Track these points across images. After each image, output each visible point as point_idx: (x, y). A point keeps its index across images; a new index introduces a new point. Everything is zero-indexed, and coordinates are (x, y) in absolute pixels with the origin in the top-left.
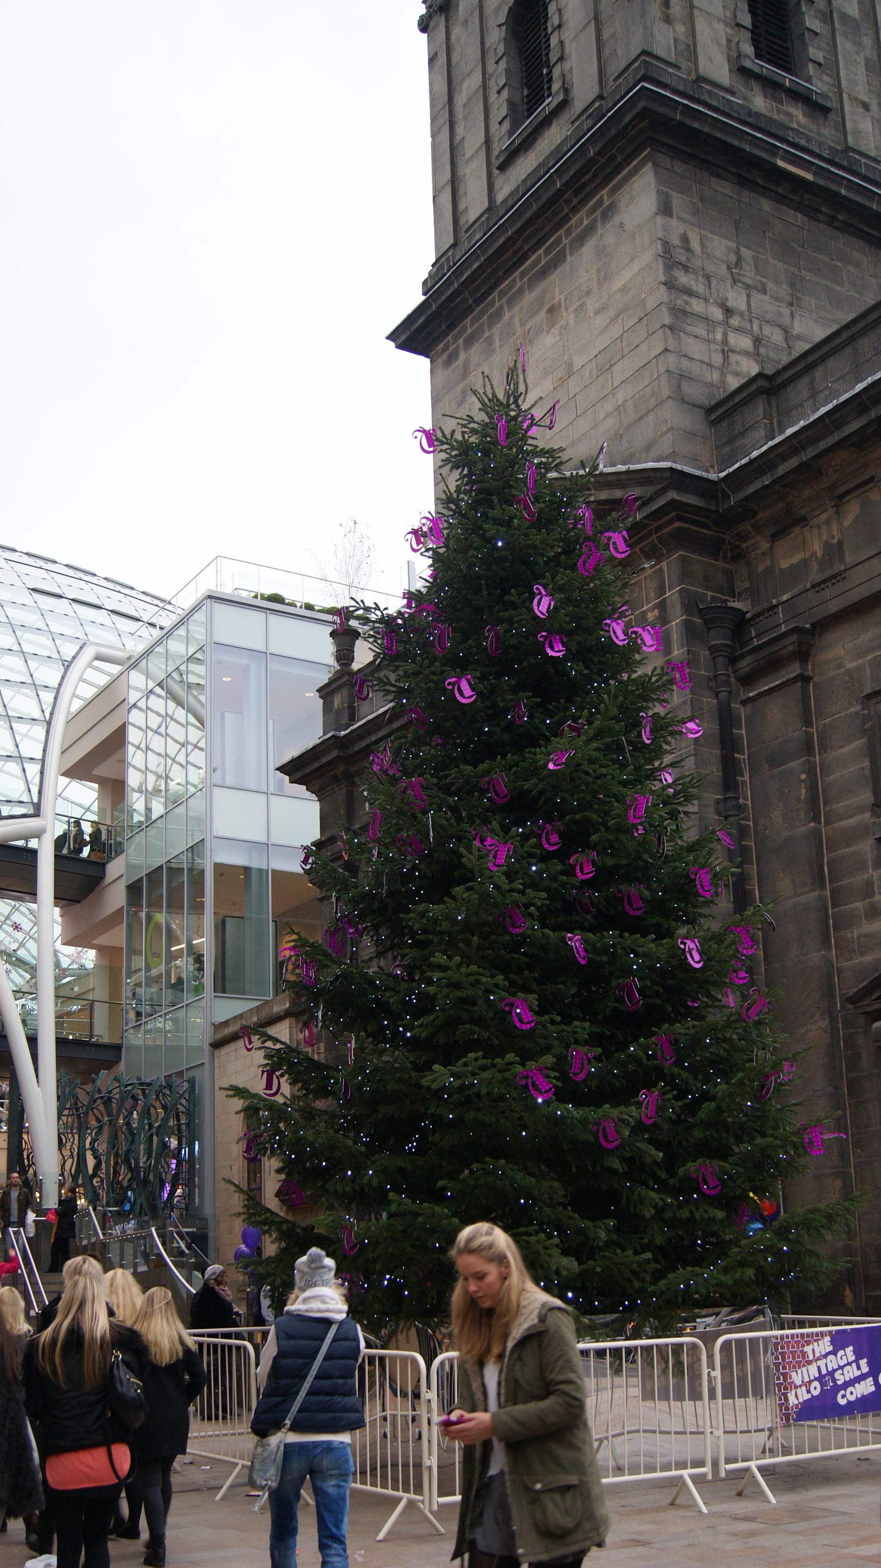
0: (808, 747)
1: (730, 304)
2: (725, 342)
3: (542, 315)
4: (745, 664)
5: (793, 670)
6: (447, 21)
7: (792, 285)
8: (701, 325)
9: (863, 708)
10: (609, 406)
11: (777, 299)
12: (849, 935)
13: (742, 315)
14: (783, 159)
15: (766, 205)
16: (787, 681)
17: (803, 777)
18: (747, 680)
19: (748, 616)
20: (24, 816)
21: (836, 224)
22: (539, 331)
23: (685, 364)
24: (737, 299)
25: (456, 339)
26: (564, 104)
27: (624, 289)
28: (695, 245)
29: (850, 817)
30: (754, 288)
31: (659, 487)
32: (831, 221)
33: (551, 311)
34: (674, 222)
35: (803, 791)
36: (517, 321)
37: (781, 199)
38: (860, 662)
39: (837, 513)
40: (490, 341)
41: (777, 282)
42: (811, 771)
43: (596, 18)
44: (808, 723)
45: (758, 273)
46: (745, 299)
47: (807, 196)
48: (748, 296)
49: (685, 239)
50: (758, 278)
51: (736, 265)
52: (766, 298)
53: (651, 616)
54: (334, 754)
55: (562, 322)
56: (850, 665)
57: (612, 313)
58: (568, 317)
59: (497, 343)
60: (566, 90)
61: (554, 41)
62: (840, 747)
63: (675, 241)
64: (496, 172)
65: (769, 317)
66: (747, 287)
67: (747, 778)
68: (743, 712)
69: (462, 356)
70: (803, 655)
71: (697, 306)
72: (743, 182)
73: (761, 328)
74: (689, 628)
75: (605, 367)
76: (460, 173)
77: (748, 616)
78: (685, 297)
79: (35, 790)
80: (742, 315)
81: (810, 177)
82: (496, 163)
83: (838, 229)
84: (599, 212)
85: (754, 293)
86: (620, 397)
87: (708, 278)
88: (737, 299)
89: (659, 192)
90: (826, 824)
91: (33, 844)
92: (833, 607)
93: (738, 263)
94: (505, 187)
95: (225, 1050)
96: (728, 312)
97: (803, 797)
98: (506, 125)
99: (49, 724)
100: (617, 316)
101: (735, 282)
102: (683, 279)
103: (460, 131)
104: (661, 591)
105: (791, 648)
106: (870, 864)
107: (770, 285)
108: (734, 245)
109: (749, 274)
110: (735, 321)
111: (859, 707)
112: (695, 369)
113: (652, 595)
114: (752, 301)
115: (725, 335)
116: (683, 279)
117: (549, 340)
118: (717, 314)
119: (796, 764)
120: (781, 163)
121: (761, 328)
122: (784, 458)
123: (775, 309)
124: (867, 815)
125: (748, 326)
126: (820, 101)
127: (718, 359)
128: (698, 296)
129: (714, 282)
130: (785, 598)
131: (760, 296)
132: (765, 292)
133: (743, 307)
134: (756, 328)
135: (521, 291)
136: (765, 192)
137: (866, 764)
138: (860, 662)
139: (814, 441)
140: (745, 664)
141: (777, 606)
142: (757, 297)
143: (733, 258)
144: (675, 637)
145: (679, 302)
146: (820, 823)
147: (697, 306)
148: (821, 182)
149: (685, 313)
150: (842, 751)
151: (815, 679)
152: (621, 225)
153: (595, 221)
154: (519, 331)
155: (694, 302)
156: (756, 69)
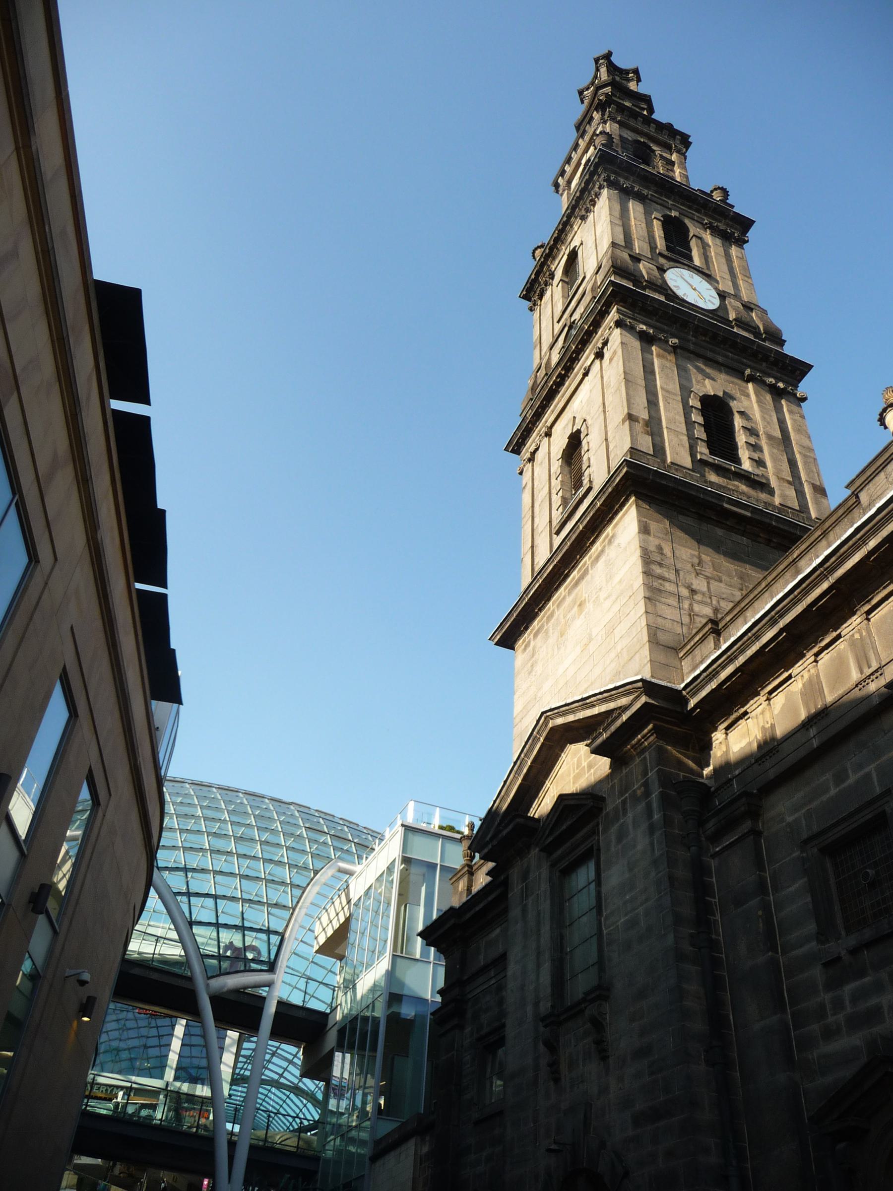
0: (762, 887)
1: (694, 587)
2: (691, 608)
3: (576, 608)
4: (711, 826)
5: (747, 825)
6: (533, 466)
7: (741, 578)
8: (672, 598)
9: (802, 852)
10: (613, 655)
11: (730, 586)
12: (810, 1057)
13: (704, 594)
14: (727, 503)
15: (720, 532)
16: (743, 835)
17: (760, 913)
18: (715, 838)
19: (713, 789)
20: (261, 971)
21: (772, 545)
22: (574, 618)
23: (660, 620)
24: (700, 584)
25: (529, 635)
26: (590, 489)
27: (620, 581)
28: (667, 551)
29: (801, 947)
30: (711, 578)
31: (633, 697)
32: (768, 542)
33: (580, 605)
34: (651, 538)
35: (761, 925)
36: (562, 617)
37: (730, 529)
38: (796, 815)
39: (769, 704)
40: (547, 632)
41: (729, 576)
42: (766, 907)
43: (606, 440)
44: (762, 868)
45: (714, 569)
46: (706, 584)
47: (748, 527)
48: (708, 583)
49: (660, 549)
50: (715, 573)
51: (699, 564)
52: (722, 585)
53: (639, 792)
54: (452, 922)
55: (586, 610)
56: (790, 819)
57: (614, 598)
58: (589, 606)
59: (551, 631)
60: (591, 482)
61: (585, 458)
62: (789, 887)
63: (652, 548)
64: (554, 536)
65: (724, 596)
66: (707, 578)
67: (718, 917)
68: (713, 864)
69: (532, 643)
70: (754, 813)
71: (669, 587)
72: (701, 518)
73: (718, 602)
74: (665, 799)
75: (610, 631)
76: (536, 543)
77: (713, 789)
78: (660, 581)
79: (272, 957)
80: (704, 594)
81: (749, 514)
82: (554, 532)
83: (774, 548)
84: (607, 541)
85: (711, 581)
86: (619, 648)
87: (677, 571)
88: (700, 584)
89: (639, 521)
90: (783, 953)
91: (263, 992)
92: (772, 774)
93: (700, 563)
94: (557, 541)
95: (379, 1163)
96: (693, 592)
97: (761, 930)
98: (561, 509)
99: (294, 909)
100: (617, 599)
101: (697, 574)
102: (658, 570)
103: (536, 520)
104: (645, 773)
105: (743, 809)
106: (847, 1003)
107: (724, 578)
108: (697, 553)
109: (709, 571)
110: (698, 597)
111: (799, 852)
112: (668, 625)
113: (640, 777)
114: (711, 586)
115: (691, 605)
116: (658, 570)
117: (578, 623)
118: (685, 592)
119: (754, 902)
120: (726, 505)
121: (718, 602)
122: (723, 667)
123: (729, 592)
124: (814, 943)
125: (709, 601)
126: (756, 478)
127: (686, 620)
128: (669, 581)
129: (681, 573)
130: (737, 772)
131: (717, 583)
132: (721, 581)
133: (705, 589)
134: (714, 602)
135: (564, 598)
136: (718, 524)
137: (809, 899)
138: (796, 815)
139: (742, 651)
140: (711, 826)
141: (731, 780)
142: (714, 585)
143: (696, 561)
144: (655, 805)
145: (655, 584)
146: (778, 953)
147: (669, 587)
148: (756, 517)
149: (660, 590)
150: (791, 889)
151: (765, 834)
152: (619, 545)
153: (604, 546)
154: (563, 621)
155: (667, 584)
156: (710, 460)
